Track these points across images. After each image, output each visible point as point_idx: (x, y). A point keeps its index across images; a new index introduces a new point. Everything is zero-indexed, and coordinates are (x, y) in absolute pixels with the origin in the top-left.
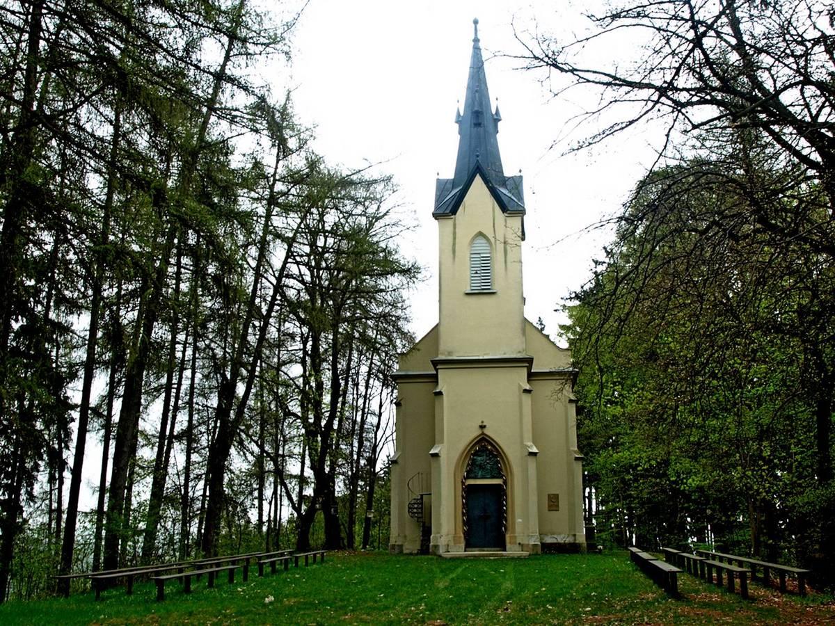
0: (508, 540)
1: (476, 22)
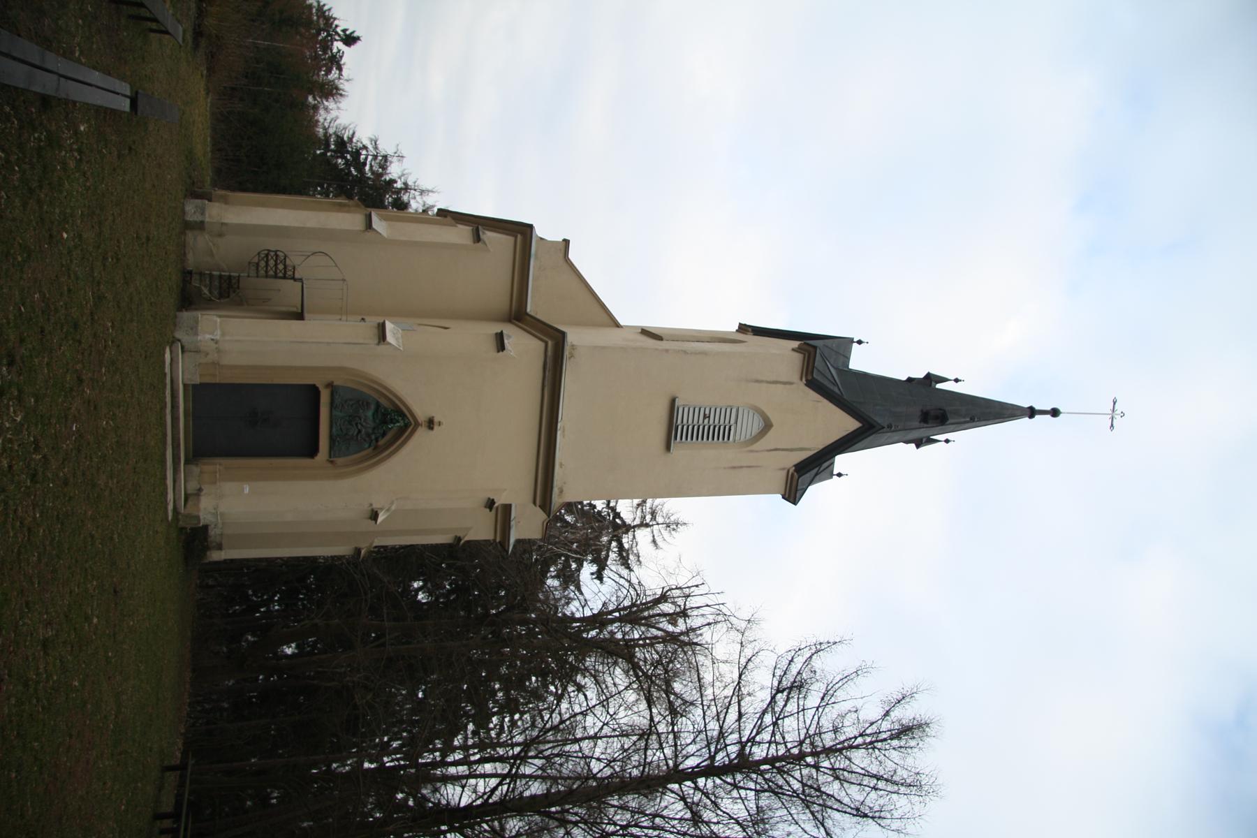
1: (1055, 413)
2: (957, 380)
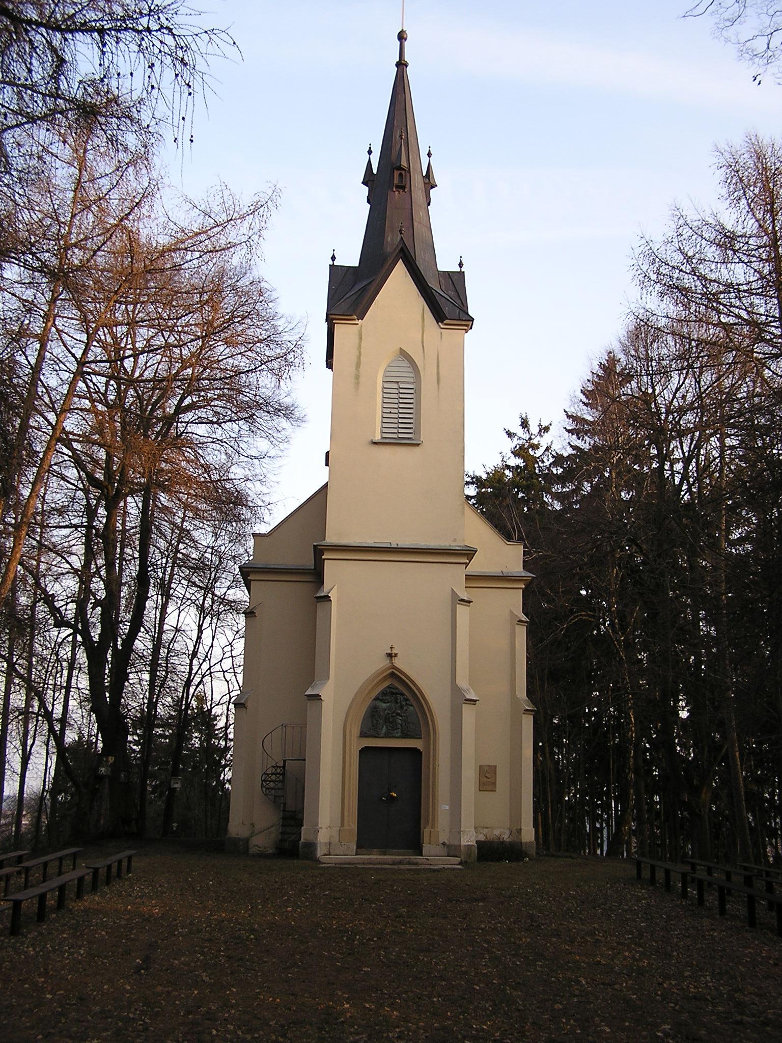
0: (426, 838)
1: (402, 37)
2: (370, 152)
